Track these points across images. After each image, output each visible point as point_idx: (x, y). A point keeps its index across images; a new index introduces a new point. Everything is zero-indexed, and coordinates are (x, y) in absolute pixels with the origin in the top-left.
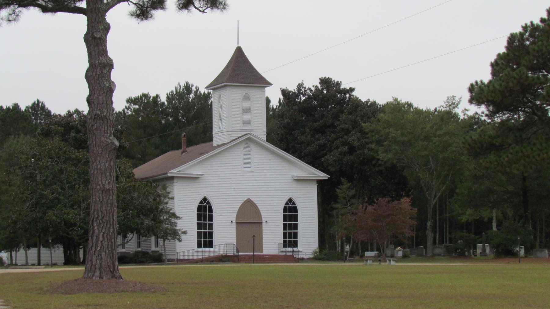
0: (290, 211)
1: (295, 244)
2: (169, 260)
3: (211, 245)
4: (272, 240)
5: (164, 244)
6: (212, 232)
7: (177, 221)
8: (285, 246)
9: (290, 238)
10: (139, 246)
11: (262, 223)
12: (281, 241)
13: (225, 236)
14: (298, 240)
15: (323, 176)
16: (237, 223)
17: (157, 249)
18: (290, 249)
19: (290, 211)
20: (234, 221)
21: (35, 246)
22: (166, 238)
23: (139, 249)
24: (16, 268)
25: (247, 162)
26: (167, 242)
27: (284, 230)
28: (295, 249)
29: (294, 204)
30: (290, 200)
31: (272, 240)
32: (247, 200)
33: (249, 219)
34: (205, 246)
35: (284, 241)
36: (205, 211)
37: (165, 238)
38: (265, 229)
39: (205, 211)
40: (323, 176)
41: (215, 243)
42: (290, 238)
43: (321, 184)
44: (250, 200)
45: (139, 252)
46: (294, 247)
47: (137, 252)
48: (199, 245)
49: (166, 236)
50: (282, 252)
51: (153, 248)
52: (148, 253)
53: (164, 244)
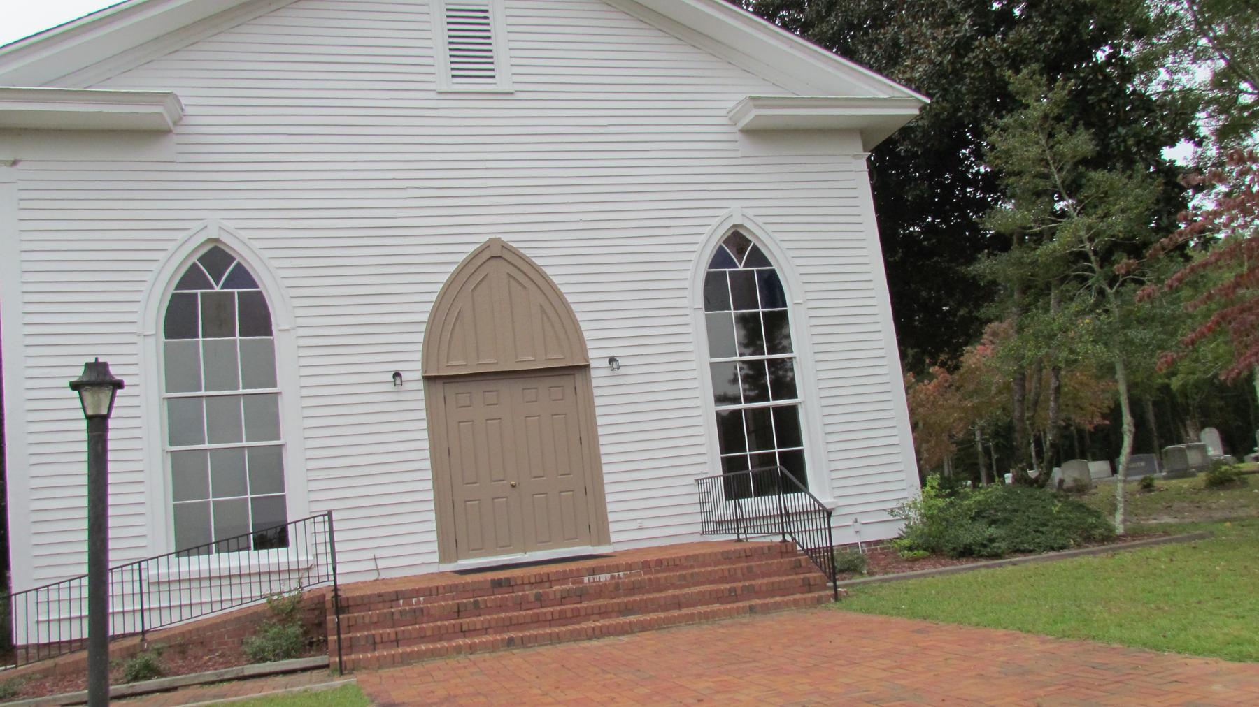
0: (748, 293)
1: (789, 474)
8: (735, 489)
9: (761, 444)
11: (585, 368)
12: (711, 460)
14: (806, 446)
16: (428, 379)
18: (767, 504)
19: (748, 293)
20: (414, 373)
21: (76, 641)
24: (660, 548)
28: (794, 501)
29: (758, 257)
30: (738, 240)
31: (655, 473)
32: (486, 246)
33: (503, 365)
35: (728, 465)
38: (609, 401)
40: (892, 100)
42: (761, 444)
44: (504, 246)
46: (790, 488)
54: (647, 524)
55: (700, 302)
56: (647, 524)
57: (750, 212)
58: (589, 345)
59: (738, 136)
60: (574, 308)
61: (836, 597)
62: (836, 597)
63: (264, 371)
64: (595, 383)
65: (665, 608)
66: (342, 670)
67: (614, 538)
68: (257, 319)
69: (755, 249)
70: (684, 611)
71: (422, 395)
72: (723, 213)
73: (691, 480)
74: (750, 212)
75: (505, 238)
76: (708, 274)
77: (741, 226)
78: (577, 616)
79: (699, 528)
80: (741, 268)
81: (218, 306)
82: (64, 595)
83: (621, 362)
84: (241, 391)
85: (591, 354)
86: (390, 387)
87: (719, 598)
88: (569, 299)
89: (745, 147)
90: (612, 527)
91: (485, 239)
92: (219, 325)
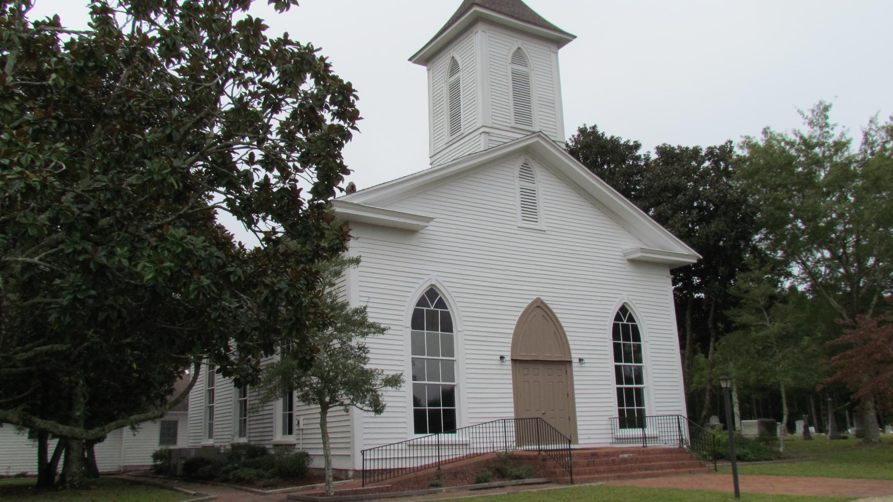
0: (626, 333)
2: (372, 325)
3: (450, 427)
4: (595, 421)
5: (323, 424)
6: (454, 411)
7: (371, 341)
9: (631, 408)
10: (242, 433)
11: (570, 362)
13: (487, 413)
15: (685, 253)
16: (512, 360)
17: (290, 439)
19: (626, 333)
20: (508, 358)
22: (333, 400)
23: (243, 440)
25: (529, 207)
26: (334, 412)
27: (617, 383)
31: (595, 421)
34: (435, 430)
35: (621, 412)
36: (432, 315)
37: (324, 398)
38: (580, 377)
39: (432, 315)
40: (685, 253)
41: (461, 420)
42: (631, 408)
43: (680, 274)
44: (542, 302)
45: (245, 446)
47: (235, 447)
48: (419, 428)
49: (333, 393)
50: (619, 440)
51: (279, 437)
52: (264, 451)
53: (323, 424)
54: (592, 436)
55: (409, 325)
56: (592, 436)
57: (440, 279)
58: (572, 351)
59: (626, 262)
60: (567, 334)
61: (716, 470)
62: (716, 470)
63: (449, 349)
64: (574, 369)
65: (657, 469)
66: (572, 482)
67: (580, 442)
68: (448, 326)
69: (441, 300)
70: (665, 471)
71: (510, 367)
72: (621, 296)
73: (607, 418)
74: (630, 297)
75: (542, 298)
76: (415, 310)
77: (434, 285)
78: (632, 469)
79: (611, 441)
80: (432, 308)
81: (432, 315)
82: (400, 448)
83: (586, 361)
84: (441, 358)
85: (573, 356)
86: (499, 362)
87: (675, 467)
88: (565, 329)
89: (628, 268)
90: (579, 437)
91: (535, 297)
92: (432, 326)
